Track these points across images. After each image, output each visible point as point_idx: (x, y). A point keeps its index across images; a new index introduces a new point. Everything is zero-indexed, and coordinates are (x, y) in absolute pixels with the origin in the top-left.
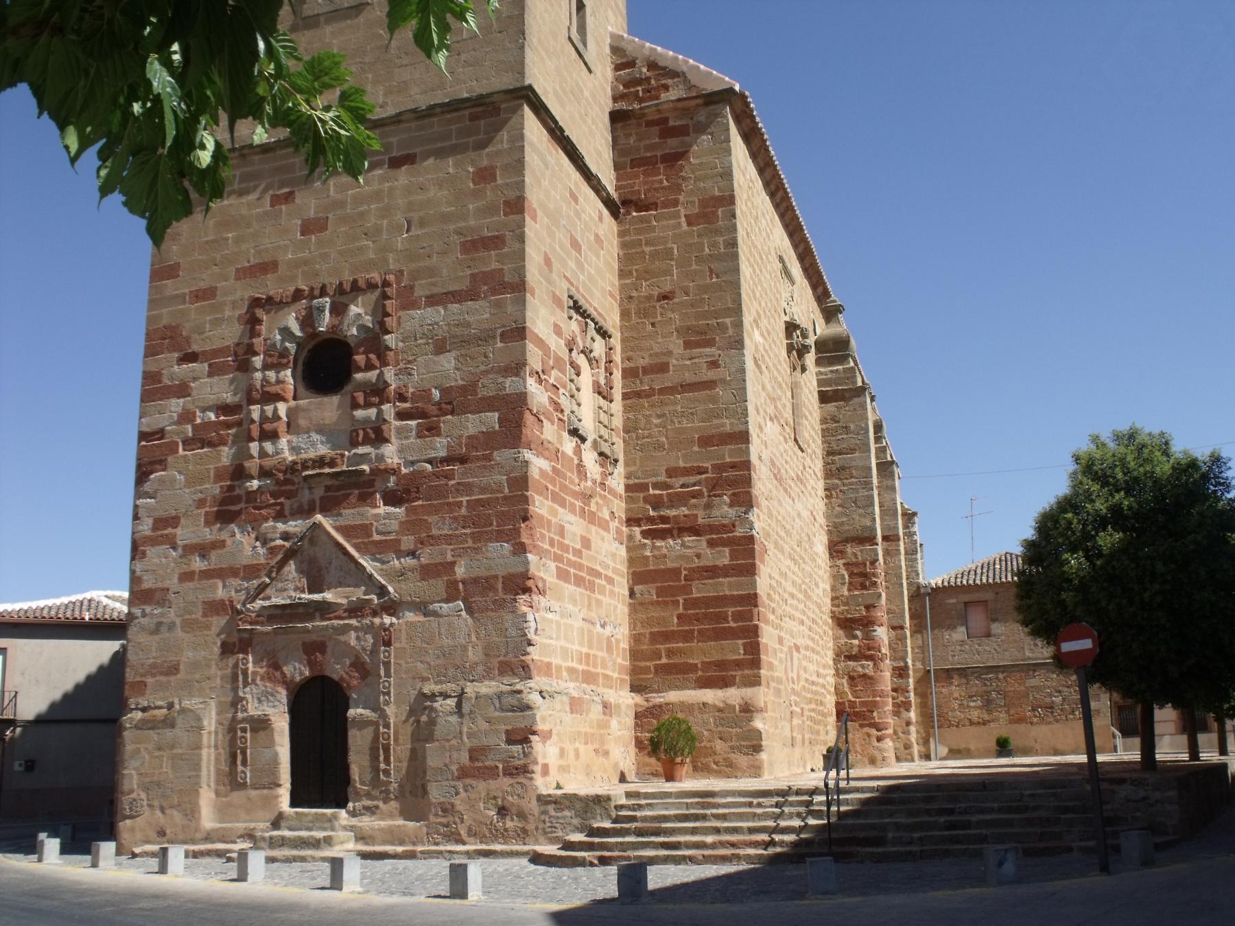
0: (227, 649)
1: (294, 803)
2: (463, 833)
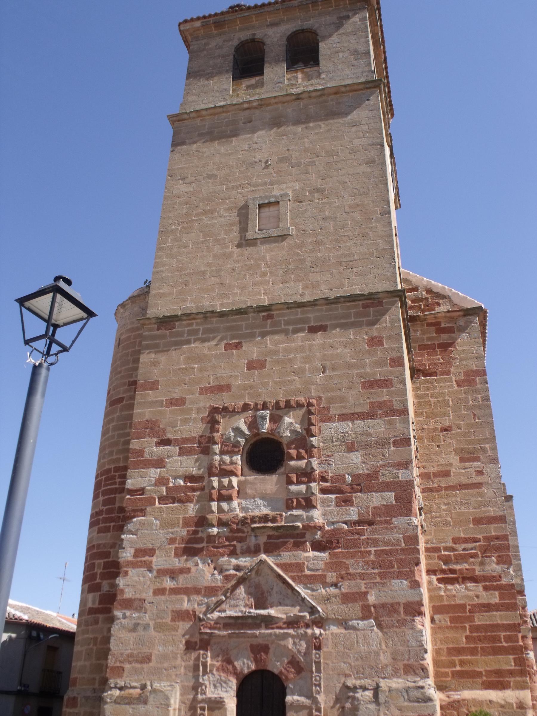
0: (190, 646)
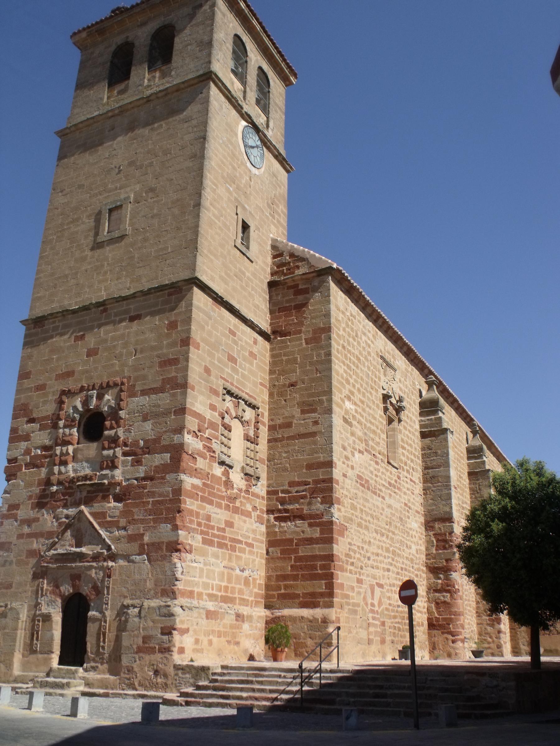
0: (36, 576)
1: (60, 663)
2: (136, 684)
